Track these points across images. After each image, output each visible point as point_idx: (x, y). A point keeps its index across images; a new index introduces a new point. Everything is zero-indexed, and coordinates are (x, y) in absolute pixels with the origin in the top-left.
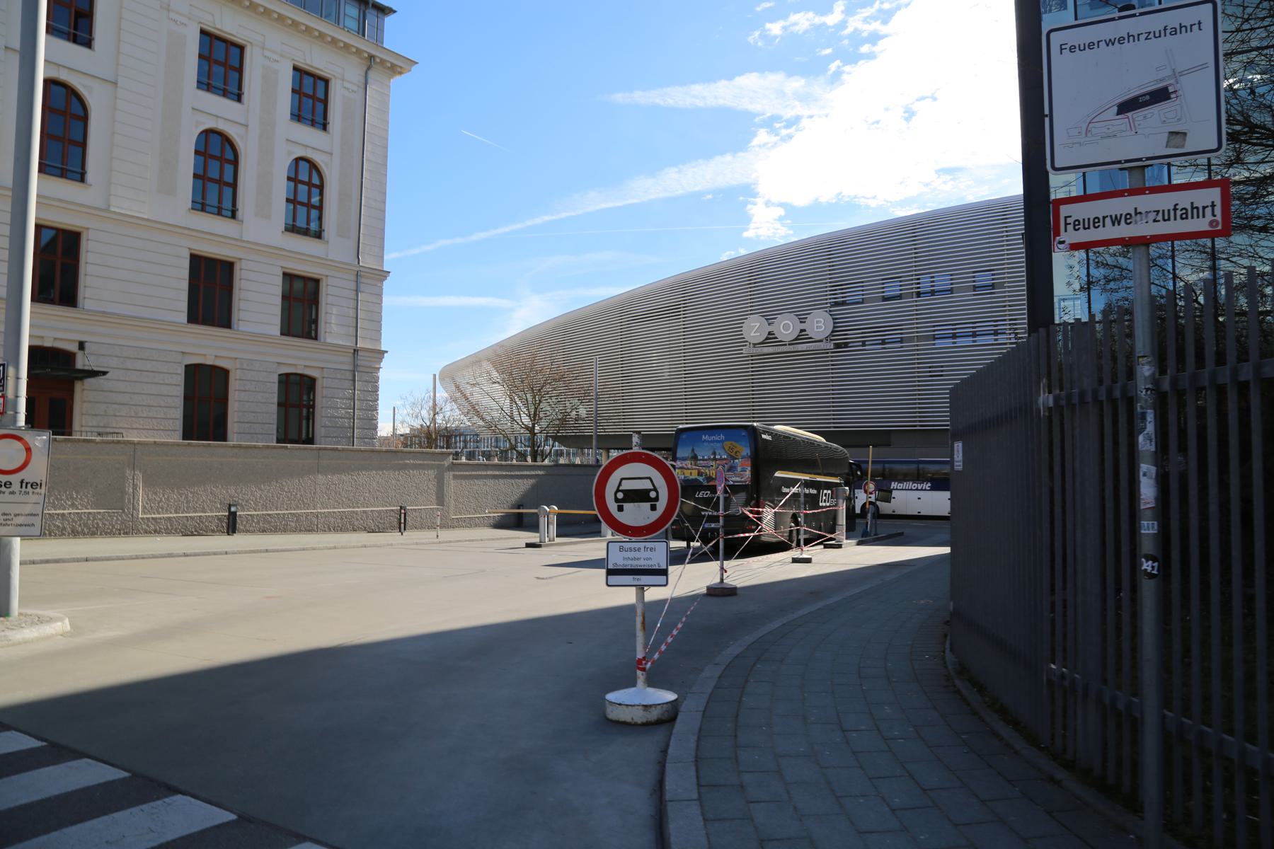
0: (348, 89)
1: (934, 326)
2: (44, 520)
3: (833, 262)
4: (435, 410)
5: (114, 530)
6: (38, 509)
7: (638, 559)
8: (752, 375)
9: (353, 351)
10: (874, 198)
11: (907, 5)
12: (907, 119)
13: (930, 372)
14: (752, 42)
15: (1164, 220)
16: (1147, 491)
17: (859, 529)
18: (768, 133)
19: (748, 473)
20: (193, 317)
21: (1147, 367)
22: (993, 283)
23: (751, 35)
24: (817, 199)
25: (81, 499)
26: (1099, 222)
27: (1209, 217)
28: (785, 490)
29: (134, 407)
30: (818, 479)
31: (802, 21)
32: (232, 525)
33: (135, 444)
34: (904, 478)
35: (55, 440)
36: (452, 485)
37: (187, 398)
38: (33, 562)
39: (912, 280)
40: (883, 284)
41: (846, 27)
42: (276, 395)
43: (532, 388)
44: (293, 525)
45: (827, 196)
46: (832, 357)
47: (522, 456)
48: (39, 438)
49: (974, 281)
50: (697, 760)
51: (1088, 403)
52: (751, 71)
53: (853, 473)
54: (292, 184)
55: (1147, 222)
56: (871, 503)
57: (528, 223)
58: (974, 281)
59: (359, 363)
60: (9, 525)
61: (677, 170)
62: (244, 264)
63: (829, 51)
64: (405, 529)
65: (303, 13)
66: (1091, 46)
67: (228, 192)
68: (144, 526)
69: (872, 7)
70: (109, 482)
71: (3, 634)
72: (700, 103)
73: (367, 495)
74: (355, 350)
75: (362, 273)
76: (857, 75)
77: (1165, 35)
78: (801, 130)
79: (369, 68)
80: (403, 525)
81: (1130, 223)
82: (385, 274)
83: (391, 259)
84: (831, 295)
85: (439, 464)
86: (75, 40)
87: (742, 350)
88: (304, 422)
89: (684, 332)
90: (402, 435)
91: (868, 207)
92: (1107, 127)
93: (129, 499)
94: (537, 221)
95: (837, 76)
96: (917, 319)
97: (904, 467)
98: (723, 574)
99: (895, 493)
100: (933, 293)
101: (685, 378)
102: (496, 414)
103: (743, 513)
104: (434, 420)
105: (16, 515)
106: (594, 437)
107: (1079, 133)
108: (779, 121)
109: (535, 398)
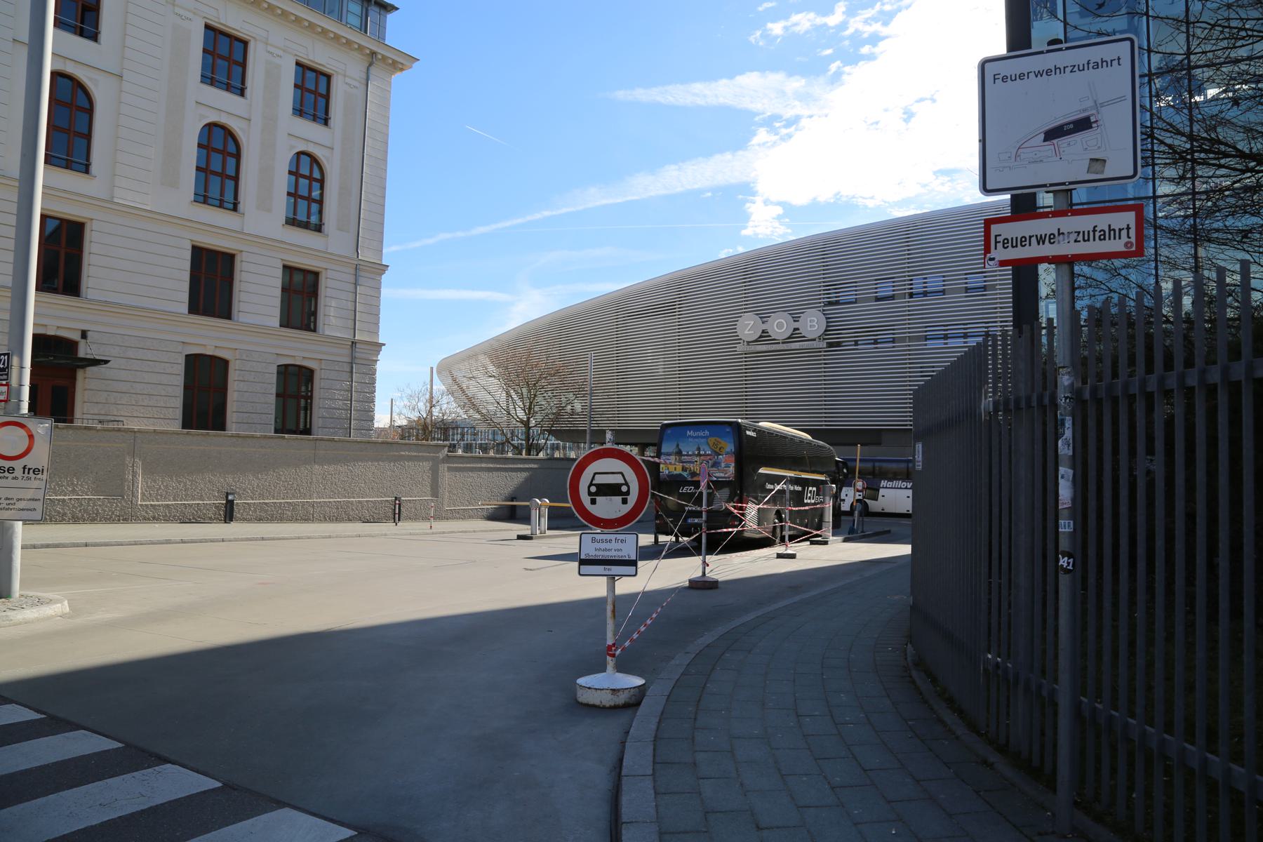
0: (349, 85)
1: (926, 327)
2: (45, 506)
3: (827, 262)
4: (432, 403)
5: (113, 516)
6: (40, 495)
7: (609, 550)
8: (746, 373)
9: (350, 343)
10: (872, 198)
11: (908, 7)
12: (907, 121)
13: (921, 372)
14: (753, 41)
15: (1084, 240)
16: (1065, 492)
17: (845, 525)
18: (768, 132)
19: (732, 469)
20: (194, 308)
21: (1066, 377)
22: (985, 285)
23: (752, 35)
24: (815, 199)
25: (82, 485)
26: (1025, 241)
27: (1124, 239)
28: (769, 486)
29: (134, 396)
30: (803, 476)
31: (804, 21)
32: (229, 514)
33: (135, 432)
34: (893, 476)
35: (57, 427)
36: (446, 477)
37: (187, 387)
38: (34, 547)
39: (905, 281)
40: (876, 284)
41: (847, 28)
42: (275, 386)
43: (527, 383)
44: (290, 514)
45: (825, 195)
46: (825, 355)
47: (517, 449)
48: (42, 425)
49: (966, 283)
50: (656, 739)
51: (1034, 407)
52: (752, 71)
53: (839, 470)
54: (293, 178)
55: (1069, 242)
56: (858, 501)
57: (529, 218)
58: (966, 283)
59: (357, 355)
60: (11, 509)
61: (677, 167)
62: (245, 256)
63: (829, 52)
64: (399, 520)
65: (306, 9)
66: (1021, 76)
67: (230, 184)
68: (144, 513)
69: (873, 9)
70: (110, 470)
71: (4, 614)
72: (700, 102)
73: (363, 485)
74: (353, 342)
75: (361, 267)
76: (857, 75)
77: (1088, 69)
78: (800, 130)
79: (370, 65)
80: (397, 516)
81: (1054, 242)
82: (381, 271)
83: (390, 252)
84: (824, 294)
85: (434, 456)
86: (82, 33)
87: (736, 347)
88: (302, 413)
89: (679, 329)
90: (399, 427)
91: (866, 207)
92: (1034, 153)
93: (129, 486)
94: (538, 216)
95: (838, 76)
96: (909, 319)
97: (894, 466)
98: (705, 568)
99: (882, 492)
100: (925, 294)
101: (679, 374)
102: (491, 408)
103: (726, 508)
104: (430, 412)
105: (19, 500)
106: (588, 432)
107: (1009, 157)
108: (779, 120)
109: (530, 392)
